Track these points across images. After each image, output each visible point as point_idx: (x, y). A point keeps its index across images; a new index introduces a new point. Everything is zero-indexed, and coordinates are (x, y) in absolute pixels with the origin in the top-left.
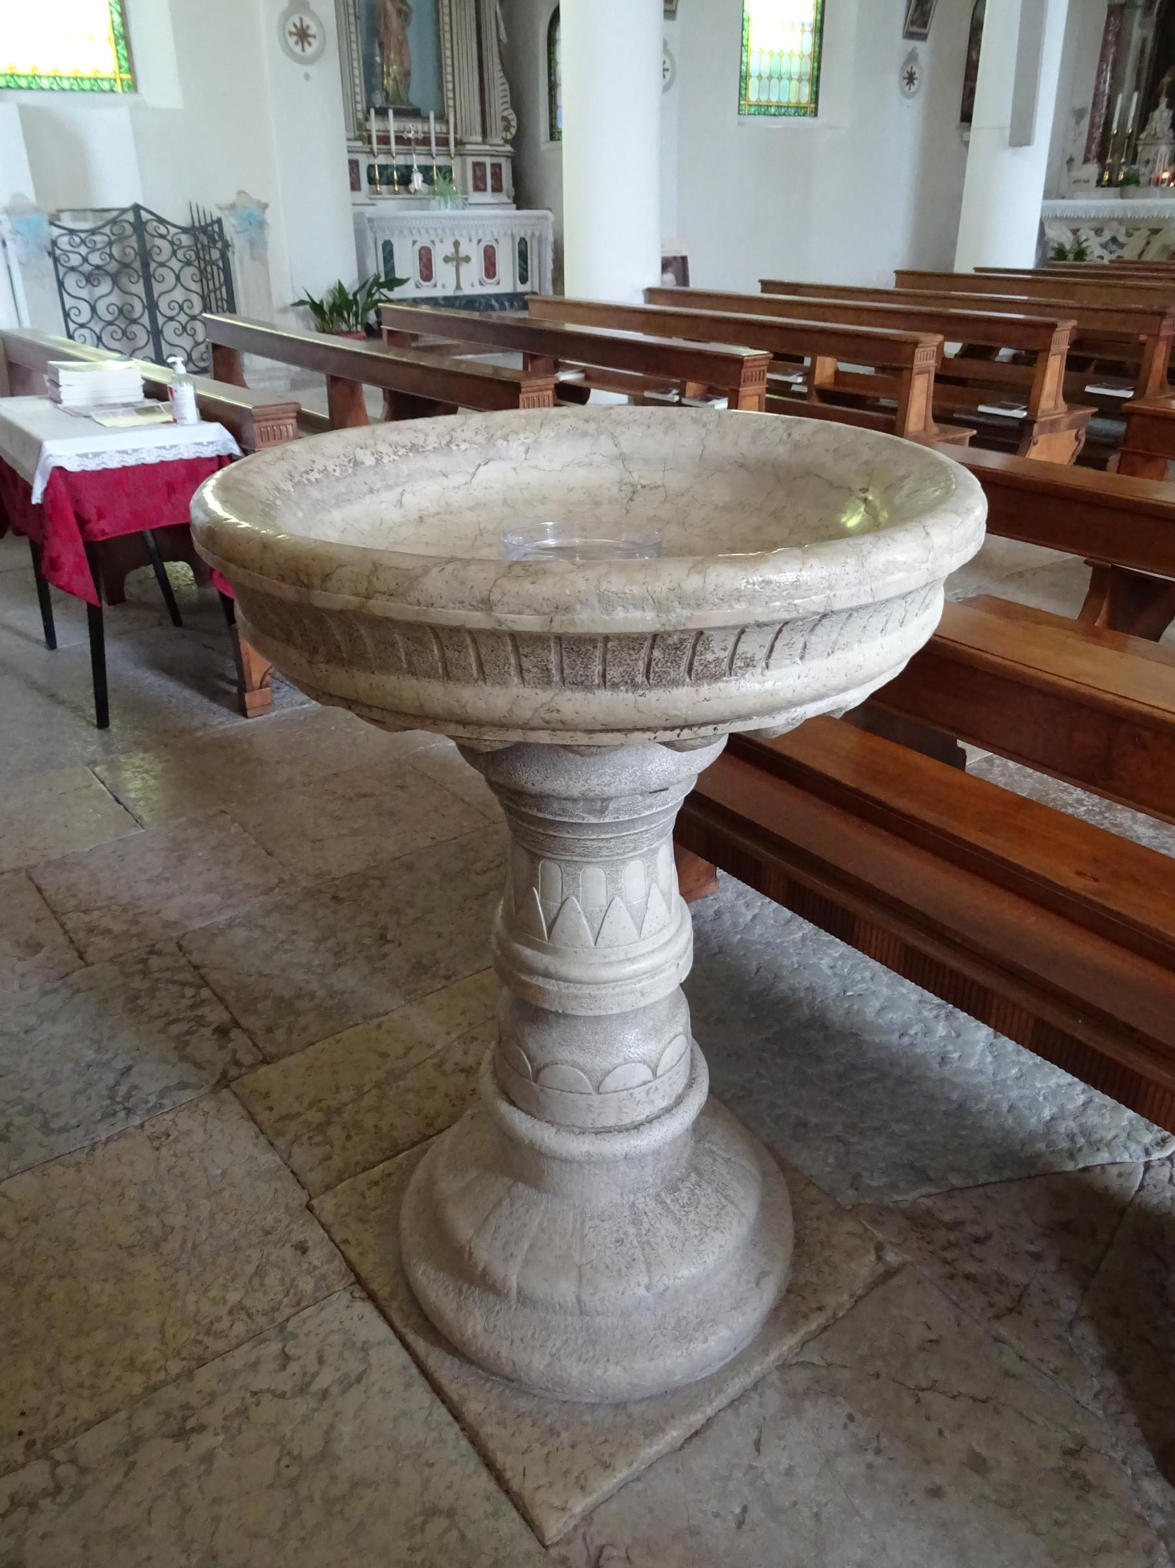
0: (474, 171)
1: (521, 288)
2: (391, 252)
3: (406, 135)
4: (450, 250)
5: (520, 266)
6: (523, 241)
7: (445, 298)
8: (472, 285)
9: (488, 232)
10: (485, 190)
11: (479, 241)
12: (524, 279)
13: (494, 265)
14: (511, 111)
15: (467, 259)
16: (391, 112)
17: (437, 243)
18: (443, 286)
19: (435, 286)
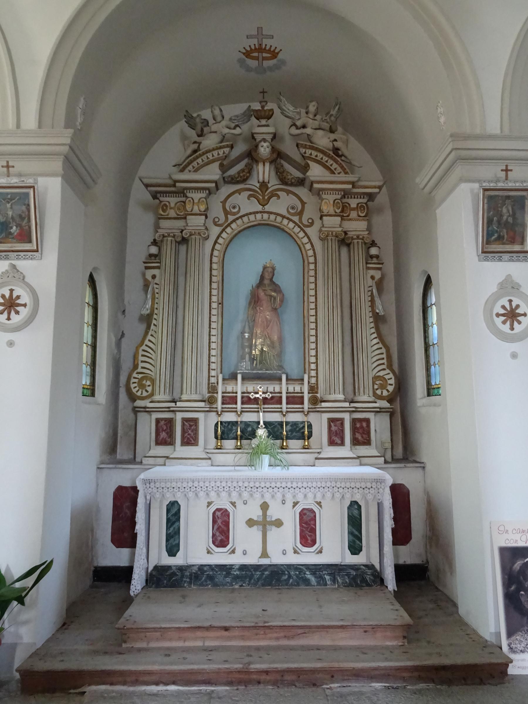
0: (330, 427)
1: (351, 559)
2: (177, 514)
3: (252, 396)
4: (256, 514)
5: (350, 533)
6: (354, 506)
7: (243, 567)
8: (284, 553)
9: (310, 495)
10: (342, 444)
11: (295, 504)
12: (355, 548)
13: (313, 531)
14: (388, 371)
15: (279, 523)
16: (239, 377)
17: (239, 504)
18: (245, 553)
19: (233, 552)
